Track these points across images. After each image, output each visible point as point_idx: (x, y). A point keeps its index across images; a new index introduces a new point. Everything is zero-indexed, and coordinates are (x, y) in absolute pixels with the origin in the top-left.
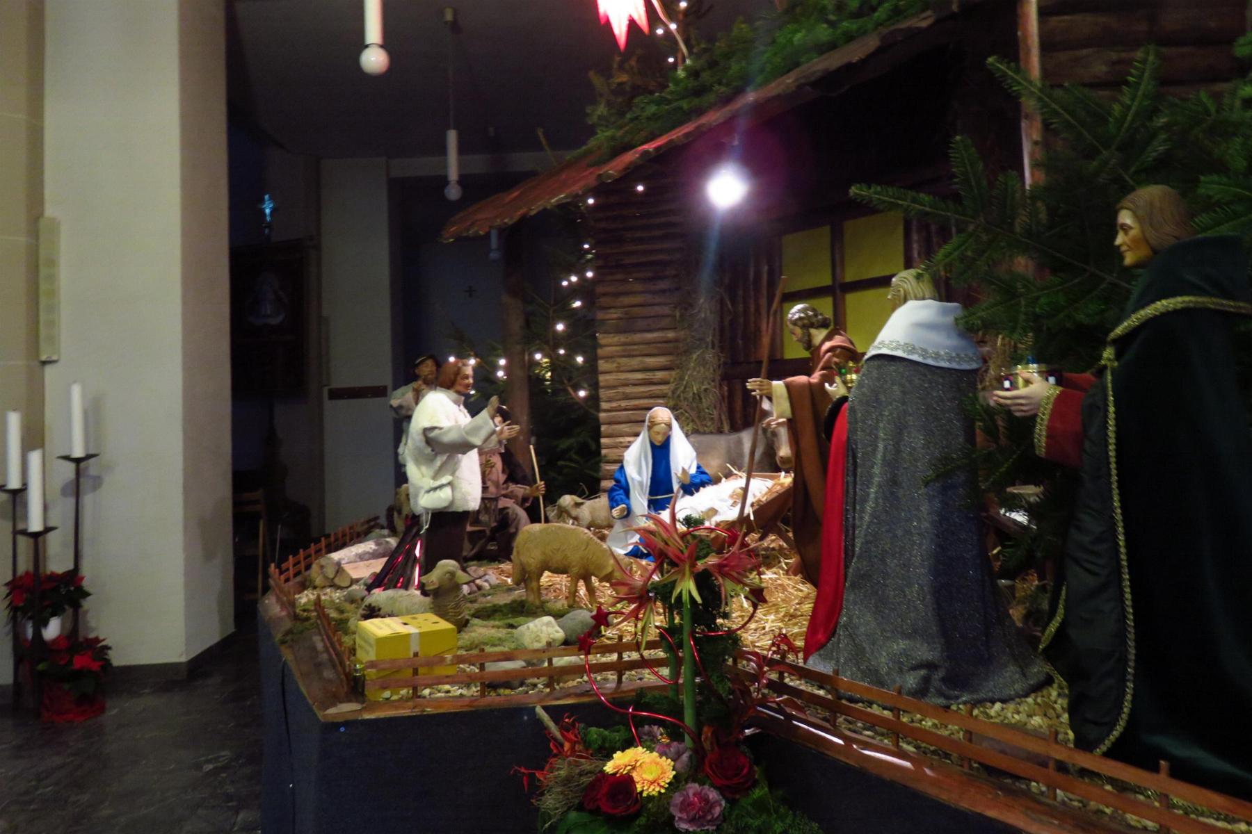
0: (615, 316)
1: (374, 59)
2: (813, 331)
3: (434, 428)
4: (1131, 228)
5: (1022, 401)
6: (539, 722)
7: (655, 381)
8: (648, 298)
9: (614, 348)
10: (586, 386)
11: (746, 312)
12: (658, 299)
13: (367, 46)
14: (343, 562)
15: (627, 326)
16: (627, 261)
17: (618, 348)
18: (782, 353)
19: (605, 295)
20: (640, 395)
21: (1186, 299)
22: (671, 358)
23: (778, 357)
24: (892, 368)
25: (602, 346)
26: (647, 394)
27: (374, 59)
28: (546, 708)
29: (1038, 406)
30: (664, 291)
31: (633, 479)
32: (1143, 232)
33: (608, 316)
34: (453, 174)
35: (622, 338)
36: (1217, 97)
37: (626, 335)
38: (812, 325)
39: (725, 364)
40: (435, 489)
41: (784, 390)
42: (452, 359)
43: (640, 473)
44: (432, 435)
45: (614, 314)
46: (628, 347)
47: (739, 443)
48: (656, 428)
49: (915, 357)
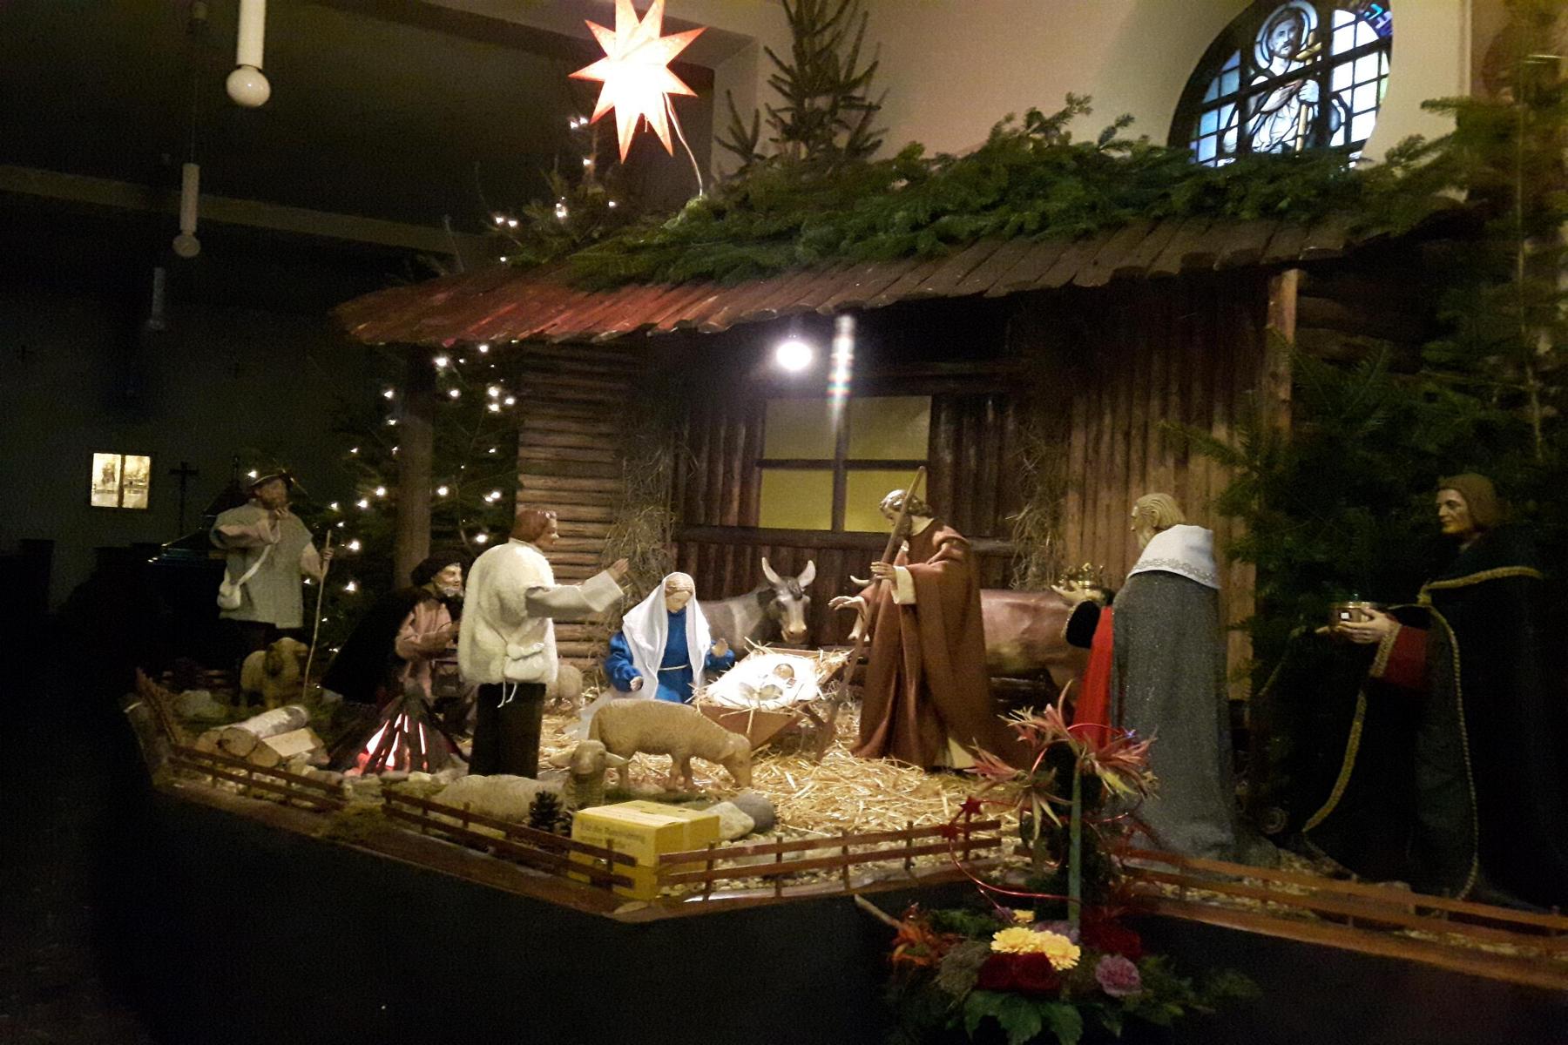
0: (543, 455)
1: (250, 86)
2: (915, 518)
3: (538, 588)
4: (1459, 505)
5: (1368, 632)
6: (861, 911)
7: (588, 534)
8: (587, 441)
9: (538, 493)
10: (487, 531)
11: (712, 472)
12: (598, 443)
13: (239, 67)
14: (261, 736)
15: (559, 468)
16: (562, 394)
17: (543, 493)
18: (757, 520)
19: (534, 430)
20: (564, 548)
21: (1526, 569)
22: (603, 510)
23: (753, 524)
24: (1189, 585)
25: (522, 487)
26: (574, 548)
27: (250, 86)
28: (864, 896)
29: (1381, 637)
30: (601, 435)
31: (637, 646)
32: (1469, 508)
33: (533, 455)
34: (189, 223)
35: (550, 482)
36: (1404, 384)
37: (554, 479)
38: (916, 513)
39: (677, 523)
40: (525, 658)
41: (910, 579)
42: (381, 492)
43: (651, 641)
44: (536, 595)
45: (539, 454)
46: (557, 493)
47: (729, 614)
48: (677, 595)
49: (1191, 576)
